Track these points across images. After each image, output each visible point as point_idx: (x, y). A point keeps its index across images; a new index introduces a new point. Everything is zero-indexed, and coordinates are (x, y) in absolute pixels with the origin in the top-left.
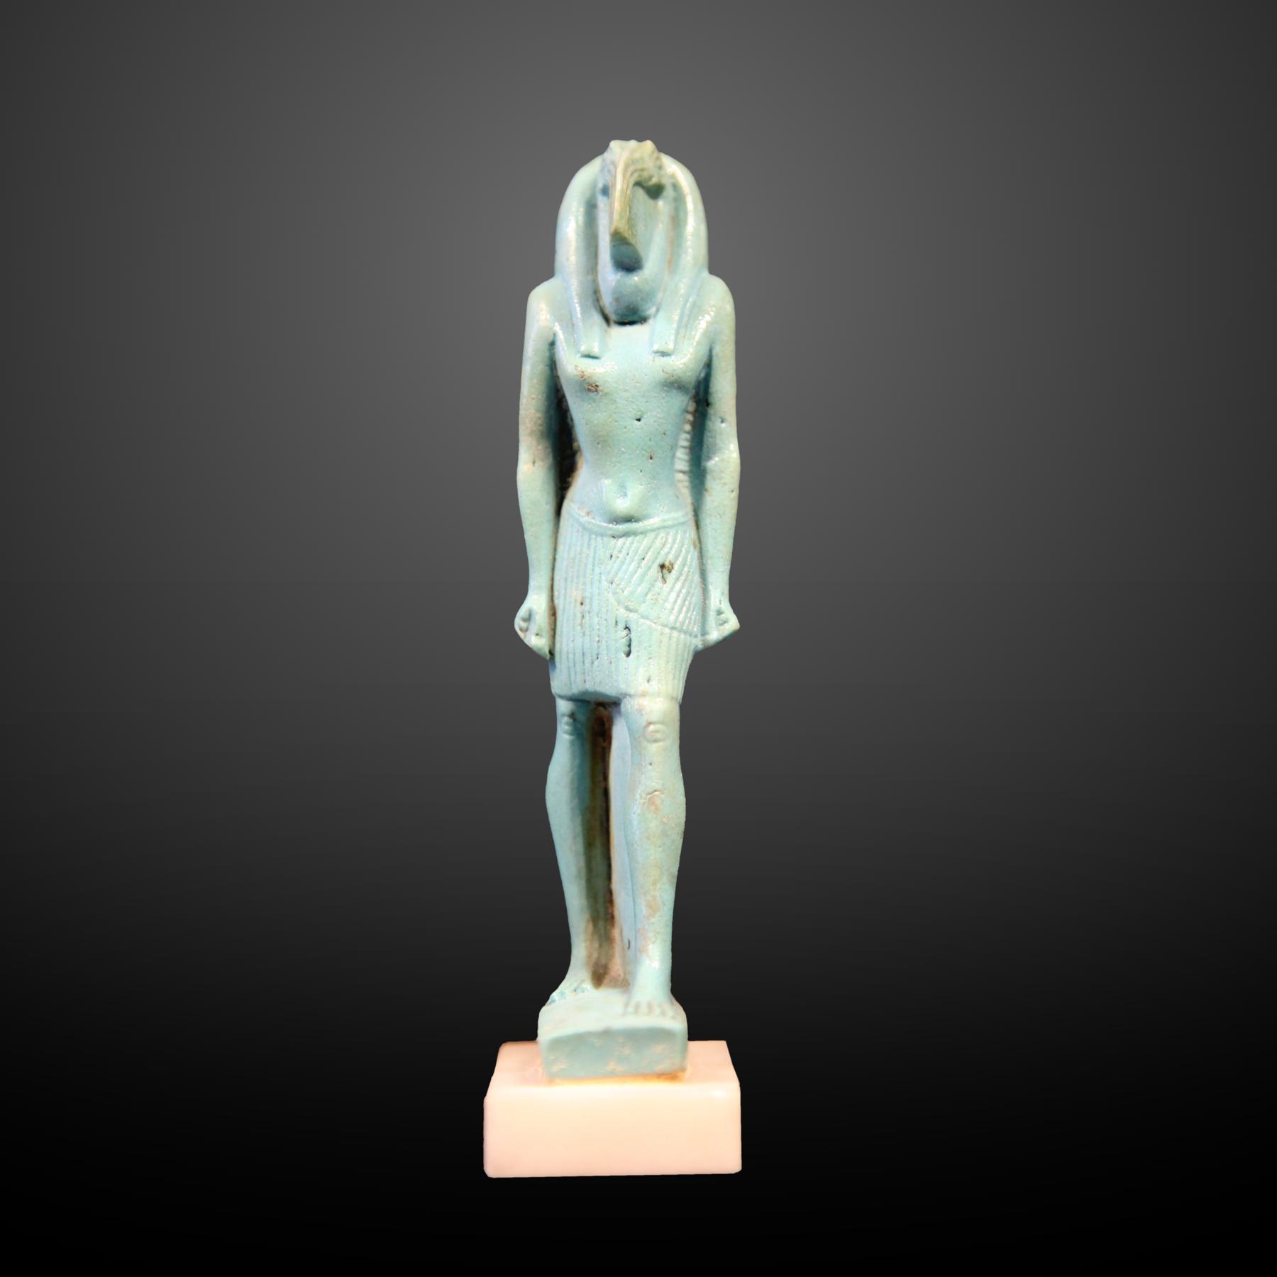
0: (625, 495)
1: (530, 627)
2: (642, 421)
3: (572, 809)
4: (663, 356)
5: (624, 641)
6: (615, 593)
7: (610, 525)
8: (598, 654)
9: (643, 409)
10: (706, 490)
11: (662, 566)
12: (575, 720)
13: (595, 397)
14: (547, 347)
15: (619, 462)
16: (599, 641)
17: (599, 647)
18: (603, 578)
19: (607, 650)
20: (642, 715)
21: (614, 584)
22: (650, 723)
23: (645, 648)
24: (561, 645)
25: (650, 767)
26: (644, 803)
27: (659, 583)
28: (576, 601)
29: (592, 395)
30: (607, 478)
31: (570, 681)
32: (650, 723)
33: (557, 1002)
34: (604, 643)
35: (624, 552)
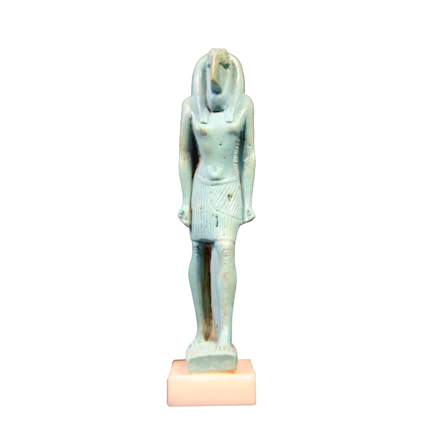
0: (216, 171)
1: (183, 217)
2: (222, 145)
3: (198, 279)
4: (229, 123)
5: (216, 221)
6: (212, 205)
7: (211, 181)
8: (206, 226)
9: (222, 141)
10: (244, 169)
11: (229, 196)
12: (198, 249)
13: (205, 137)
14: (189, 120)
15: (214, 160)
16: (207, 221)
17: (207, 223)
18: (208, 200)
19: (210, 224)
20: (222, 247)
21: (212, 202)
22: (224, 250)
23: (223, 224)
24: (194, 223)
25: (225, 265)
26: (223, 277)
27: (228, 202)
28: (199, 207)
29: (204, 136)
30: (209, 165)
31: (197, 235)
32: (224, 250)
33: (192, 346)
34: (209, 222)
35: (216, 191)
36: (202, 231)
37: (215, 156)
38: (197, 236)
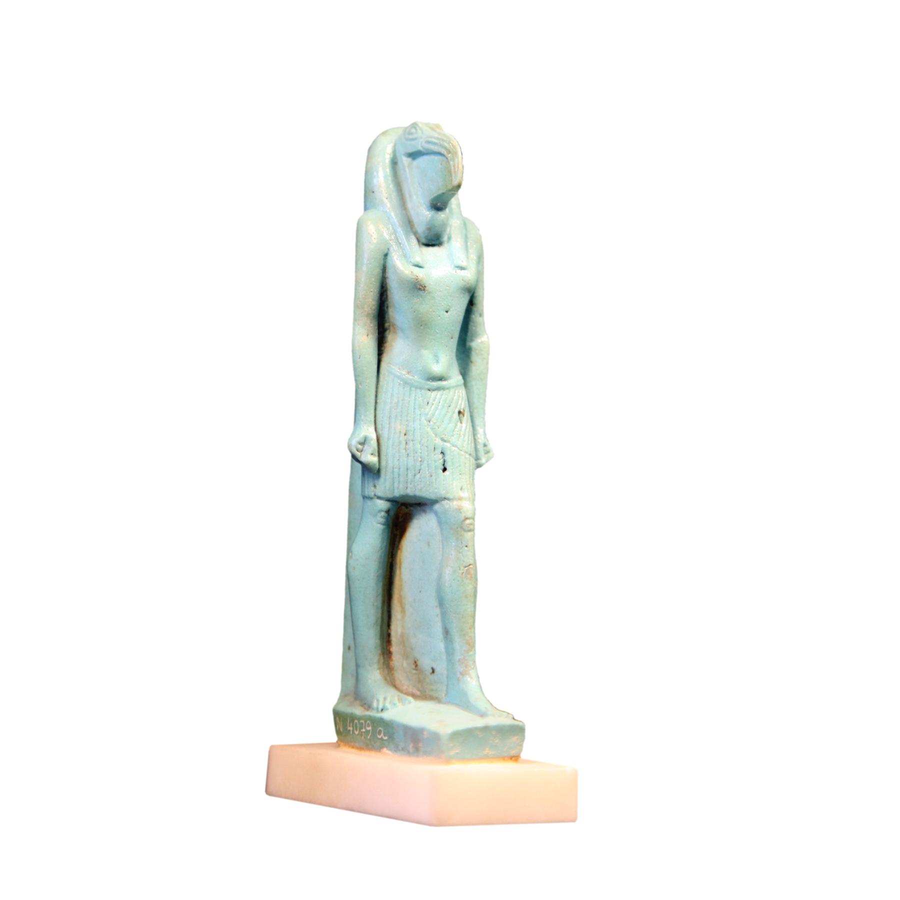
0: (437, 362)
1: (364, 449)
2: (449, 313)
3: (378, 576)
4: (461, 270)
5: (441, 461)
6: (432, 429)
7: (429, 382)
8: (420, 470)
9: (450, 304)
10: (471, 362)
11: (460, 412)
12: (388, 515)
13: (422, 294)
14: (383, 257)
15: (434, 340)
16: (421, 461)
17: (421, 465)
18: (423, 418)
19: (428, 467)
20: (461, 513)
21: (431, 422)
22: (467, 518)
23: (457, 467)
25: (466, 548)
26: (463, 573)
27: (459, 424)
28: (400, 432)
29: (421, 292)
30: (426, 350)
31: (393, 487)
32: (467, 518)
33: (390, 710)
34: (425, 462)
35: (437, 400)
36: (409, 481)
37: (437, 333)
38: (394, 490)
